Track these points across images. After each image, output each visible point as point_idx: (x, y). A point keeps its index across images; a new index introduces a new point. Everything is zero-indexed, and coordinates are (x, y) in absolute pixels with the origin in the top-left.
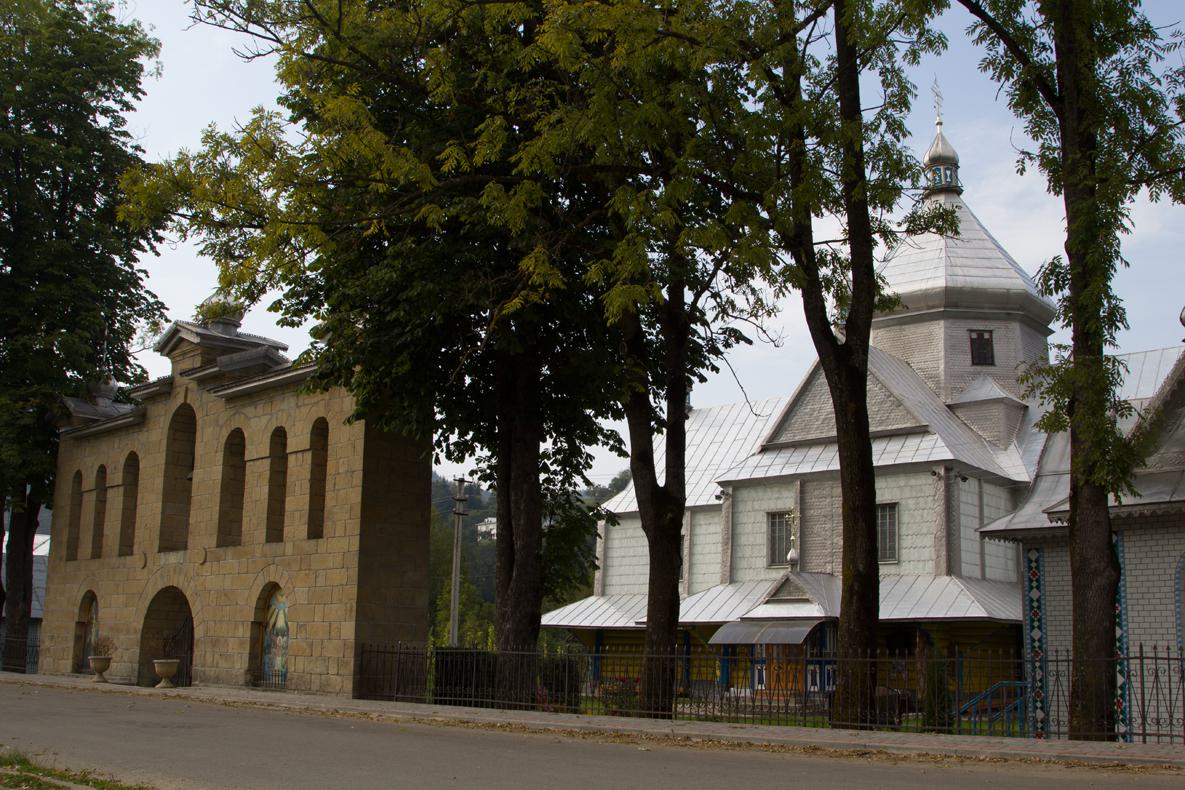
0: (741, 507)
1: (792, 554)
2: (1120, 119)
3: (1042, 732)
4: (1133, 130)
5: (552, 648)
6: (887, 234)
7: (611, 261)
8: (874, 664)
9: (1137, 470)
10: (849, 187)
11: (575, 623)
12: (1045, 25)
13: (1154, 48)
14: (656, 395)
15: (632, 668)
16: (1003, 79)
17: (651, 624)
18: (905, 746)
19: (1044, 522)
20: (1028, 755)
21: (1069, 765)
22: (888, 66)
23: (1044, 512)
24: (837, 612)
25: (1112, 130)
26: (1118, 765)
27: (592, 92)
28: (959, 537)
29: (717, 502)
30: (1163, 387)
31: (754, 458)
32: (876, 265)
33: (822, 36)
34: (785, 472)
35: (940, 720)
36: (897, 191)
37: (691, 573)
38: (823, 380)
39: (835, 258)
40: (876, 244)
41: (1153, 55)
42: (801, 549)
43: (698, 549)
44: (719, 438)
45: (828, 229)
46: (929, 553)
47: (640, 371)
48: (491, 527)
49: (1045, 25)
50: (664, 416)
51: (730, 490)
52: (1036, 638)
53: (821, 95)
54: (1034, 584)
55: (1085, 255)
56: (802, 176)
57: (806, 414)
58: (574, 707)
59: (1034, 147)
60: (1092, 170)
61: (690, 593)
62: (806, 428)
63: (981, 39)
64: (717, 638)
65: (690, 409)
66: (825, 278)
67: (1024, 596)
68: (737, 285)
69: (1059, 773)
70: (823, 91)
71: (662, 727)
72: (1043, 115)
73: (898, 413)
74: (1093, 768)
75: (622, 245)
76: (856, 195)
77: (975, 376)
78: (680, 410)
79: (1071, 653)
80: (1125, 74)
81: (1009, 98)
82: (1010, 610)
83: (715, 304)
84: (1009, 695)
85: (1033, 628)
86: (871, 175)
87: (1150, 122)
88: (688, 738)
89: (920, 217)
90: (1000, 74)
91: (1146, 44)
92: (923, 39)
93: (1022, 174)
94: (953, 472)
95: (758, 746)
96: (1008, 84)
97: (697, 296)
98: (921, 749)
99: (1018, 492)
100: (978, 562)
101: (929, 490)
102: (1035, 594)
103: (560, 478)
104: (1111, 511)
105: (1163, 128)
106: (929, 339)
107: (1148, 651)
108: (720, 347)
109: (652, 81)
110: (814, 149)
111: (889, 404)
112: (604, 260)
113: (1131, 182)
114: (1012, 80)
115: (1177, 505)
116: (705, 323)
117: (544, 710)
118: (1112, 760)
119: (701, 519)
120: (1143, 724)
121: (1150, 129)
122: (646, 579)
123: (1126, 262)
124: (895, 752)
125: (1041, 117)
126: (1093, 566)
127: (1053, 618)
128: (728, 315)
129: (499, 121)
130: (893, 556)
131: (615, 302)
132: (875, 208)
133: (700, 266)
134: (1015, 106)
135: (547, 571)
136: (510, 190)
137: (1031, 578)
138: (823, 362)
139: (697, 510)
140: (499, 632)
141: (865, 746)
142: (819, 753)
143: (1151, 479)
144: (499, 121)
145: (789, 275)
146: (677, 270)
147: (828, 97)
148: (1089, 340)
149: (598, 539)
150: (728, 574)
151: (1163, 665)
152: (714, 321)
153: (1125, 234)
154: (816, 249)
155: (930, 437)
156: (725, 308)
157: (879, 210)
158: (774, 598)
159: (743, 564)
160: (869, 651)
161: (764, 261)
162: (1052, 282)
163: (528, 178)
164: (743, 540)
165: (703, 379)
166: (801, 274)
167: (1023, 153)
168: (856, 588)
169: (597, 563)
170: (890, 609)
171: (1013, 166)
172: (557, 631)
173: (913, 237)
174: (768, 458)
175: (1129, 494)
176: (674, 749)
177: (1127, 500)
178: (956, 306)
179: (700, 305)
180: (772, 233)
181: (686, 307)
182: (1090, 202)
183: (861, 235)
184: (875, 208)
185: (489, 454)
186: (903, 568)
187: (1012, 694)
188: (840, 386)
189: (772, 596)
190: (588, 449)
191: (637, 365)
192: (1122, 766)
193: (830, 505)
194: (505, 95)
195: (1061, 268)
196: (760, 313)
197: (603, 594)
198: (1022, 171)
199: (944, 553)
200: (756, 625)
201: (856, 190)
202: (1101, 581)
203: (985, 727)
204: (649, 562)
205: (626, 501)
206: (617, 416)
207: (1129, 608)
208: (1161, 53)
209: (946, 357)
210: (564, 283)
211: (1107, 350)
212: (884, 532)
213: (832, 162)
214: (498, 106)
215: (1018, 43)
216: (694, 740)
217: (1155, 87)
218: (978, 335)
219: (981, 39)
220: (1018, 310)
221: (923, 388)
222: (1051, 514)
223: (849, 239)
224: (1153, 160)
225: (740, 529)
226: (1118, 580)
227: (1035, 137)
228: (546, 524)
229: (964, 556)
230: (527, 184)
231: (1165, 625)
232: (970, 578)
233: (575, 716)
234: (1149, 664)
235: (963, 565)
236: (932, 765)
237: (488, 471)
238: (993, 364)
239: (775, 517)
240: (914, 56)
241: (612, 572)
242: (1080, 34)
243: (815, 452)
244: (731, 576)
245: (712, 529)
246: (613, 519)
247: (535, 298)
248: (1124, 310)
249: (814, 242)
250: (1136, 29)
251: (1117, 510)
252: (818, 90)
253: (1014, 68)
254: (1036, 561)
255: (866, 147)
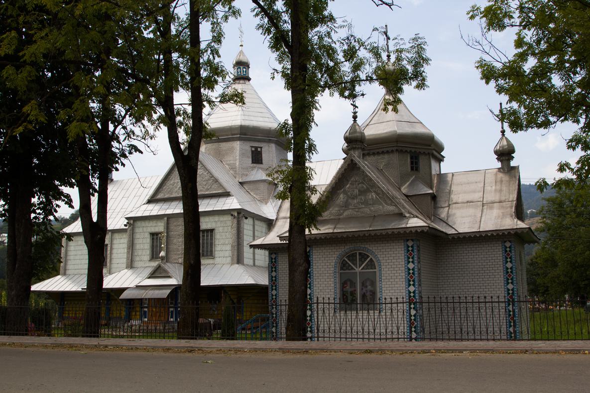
0: (137, 230)
1: (162, 254)
2: (318, 58)
3: (275, 338)
4: (324, 63)
5: (37, 303)
6: (210, 102)
7: (72, 110)
8: (197, 308)
9: (320, 218)
10: (192, 79)
11: (50, 289)
12: (287, 12)
13: (334, 28)
14: (93, 176)
15: (78, 311)
16: (267, 34)
17: (88, 290)
18: (211, 346)
19: (278, 241)
20: (266, 348)
21: (284, 352)
22: (215, 20)
23: (278, 236)
24: (181, 283)
25: (314, 63)
26: (305, 351)
27: (65, 22)
28: (243, 246)
29: (125, 228)
30: (332, 181)
31: (145, 205)
32: (204, 116)
33: (183, 5)
34: (160, 213)
35: (229, 334)
36: (216, 82)
37: (111, 263)
38: (176, 172)
39: (185, 112)
40: (205, 107)
41: (333, 31)
42: (166, 251)
43: (114, 251)
44: (127, 195)
45: (182, 98)
46: (228, 253)
47: (85, 164)
48: (4, 239)
49: (287, 12)
50: (97, 187)
51: (132, 221)
52: (274, 294)
53: (182, 32)
54: (274, 269)
55: (299, 119)
56: (169, 72)
57: (171, 184)
58: (48, 333)
59: (279, 67)
60: (304, 81)
61: (110, 273)
62: (171, 192)
63: (257, 15)
64: (124, 296)
65: (112, 180)
66: (180, 122)
67: (269, 275)
68: (136, 123)
69: (279, 356)
70: (183, 30)
71: (94, 341)
72: (284, 53)
73: (215, 186)
74: (294, 353)
75: (77, 102)
76: (196, 83)
77: (253, 168)
78: (105, 180)
79: (287, 301)
80: (321, 38)
81: (269, 43)
82: (264, 280)
83: (124, 132)
84: (262, 321)
85: (272, 290)
86: (204, 74)
87: (331, 60)
88: (106, 346)
89: (227, 95)
90: (265, 32)
91: (331, 26)
92: (231, 11)
93: (273, 79)
94: (240, 215)
95: (140, 349)
96: (269, 37)
97: (116, 127)
98: (218, 348)
99: (270, 224)
100: (252, 258)
101: (229, 223)
102: (274, 274)
103: (42, 216)
104: (306, 237)
105: (337, 64)
106: (232, 149)
107: (321, 300)
108: (127, 153)
109: (96, 19)
110: (176, 60)
111: (211, 181)
112: (68, 109)
113: (321, 87)
114: (271, 36)
115: (336, 234)
116: (119, 142)
117: (32, 335)
118: (303, 349)
119: (116, 236)
120: (318, 332)
121: (331, 64)
122: (86, 266)
123: (316, 124)
124: (205, 349)
125: (283, 54)
126: (298, 262)
127: (281, 285)
128: (131, 138)
129: (13, 33)
130: (210, 254)
131: (73, 129)
132: (205, 89)
133: (117, 112)
134: (272, 47)
135: (34, 264)
136: (19, 70)
137: (273, 266)
138: (177, 163)
139: (114, 231)
140: (8, 296)
141: (192, 347)
142: (170, 351)
143: (325, 222)
144: (13, 33)
145: (161, 120)
146: (106, 114)
147: (185, 33)
148: (300, 160)
149: (62, 248)
150: (130, 264)
151: (326, 306)
152: (124, 141)
153: (317, 111)
154: (175, 107)
155: (231, 197)
156: (129, 134)
157: (207, 90)
158: (152, 276)
159: (137, 259)
160: (195, 302)
161: (150, 109)
162: (284, 131)
163: (29, 64)
164: (137, 247)
165: (117, 170)
166: (167, 120)
167: (274, 69)
168: (190, 272)
169: (62, 260)
170: (208, 279)
171: (270, 76)
172: (39, 293)
173: (223, 105)
174: (151, 206)
175: (315, 229)
176: (99, 352)
177: (314, 231)
178: (245, 135)
179: (117, 132)
180: (153, 99)
181: (110, 133)
182: (302, 95)
183: (197, 102)
184: (205, 89)
185: (4, 203)
186: (216, 261)
187: (263, 320)
188: (184, 175)
189: (152, 274)
190: (55, 202)
191: (83, 161)
192: (306, 352)
193: (179, 229)
194: (17, 19)
195: (288, 125)
196: (147, 138)
197: (65, 274)
198: (273, 78)
199: (236, 253)
200: (144, 289)
201: (196, 81)
202: (301, 268)
203: (258, 336)
204: (87, 253)
205: (76, 227)
206: (72, 186)
207: (314, 280)
208: (336, 30)
209: (240, 159)
210: (46, 120)
211: (307, 164)
212: (203, 244)
213: (184, 67)
214: (14, 25)
215: (274, 18)
216: (110, 347)
217: (333, 45)
218: (255, 149)
219: (257, 15)
220: (274, 138)
221: (228, 174)
222: (281, 238)
223: (192, 103)
224: (331, 78)
225: (136, 241)
226: (309, 267)
227: (280, 62)
228: (34, 239)
229: (245, 255)
230: (28, 68)
231: (330, 288)
232: (248, 265)
233: (48, 338)
234: (321, 306)
235: (245, 259)
236: (223, 355)
237: (3, 212)
238: (262, 163)
239: (154, 235)
240: (226, 18)
241: (69, 263)
242: (302, 18)
243: (174, 204)
244: (131, 265)
245: (122, 241)
246: (70, 236)
247: (30, 127)
248: (315, 145)
249: (174, 104)
250: (327, 17)
251: (309, 236)
252: (180, 29)
253: (272, 30)
254: (275, 259)
255: (201, 61)
